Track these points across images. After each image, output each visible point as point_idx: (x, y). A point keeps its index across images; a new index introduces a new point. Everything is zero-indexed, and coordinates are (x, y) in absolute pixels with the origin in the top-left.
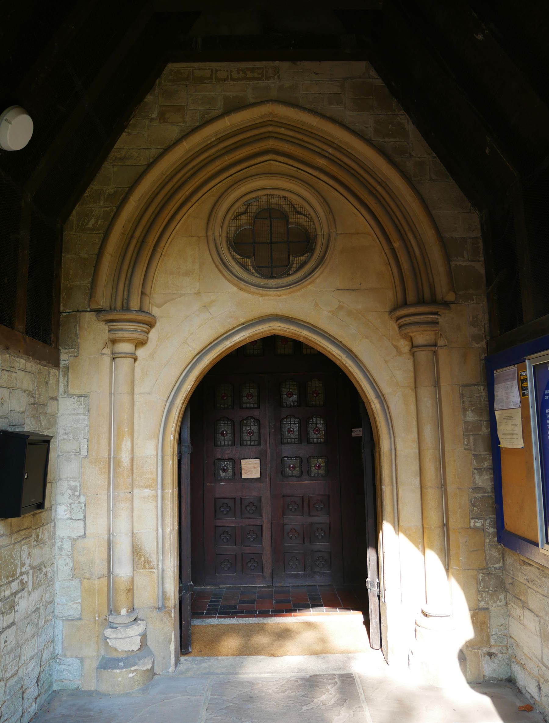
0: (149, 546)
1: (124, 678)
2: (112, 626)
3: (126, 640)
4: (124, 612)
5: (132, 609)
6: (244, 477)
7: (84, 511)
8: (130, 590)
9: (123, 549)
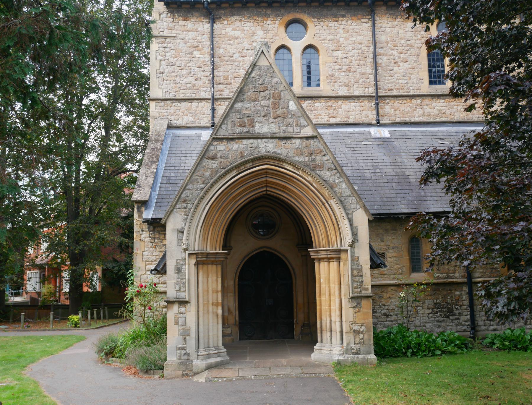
8: (228, 319)
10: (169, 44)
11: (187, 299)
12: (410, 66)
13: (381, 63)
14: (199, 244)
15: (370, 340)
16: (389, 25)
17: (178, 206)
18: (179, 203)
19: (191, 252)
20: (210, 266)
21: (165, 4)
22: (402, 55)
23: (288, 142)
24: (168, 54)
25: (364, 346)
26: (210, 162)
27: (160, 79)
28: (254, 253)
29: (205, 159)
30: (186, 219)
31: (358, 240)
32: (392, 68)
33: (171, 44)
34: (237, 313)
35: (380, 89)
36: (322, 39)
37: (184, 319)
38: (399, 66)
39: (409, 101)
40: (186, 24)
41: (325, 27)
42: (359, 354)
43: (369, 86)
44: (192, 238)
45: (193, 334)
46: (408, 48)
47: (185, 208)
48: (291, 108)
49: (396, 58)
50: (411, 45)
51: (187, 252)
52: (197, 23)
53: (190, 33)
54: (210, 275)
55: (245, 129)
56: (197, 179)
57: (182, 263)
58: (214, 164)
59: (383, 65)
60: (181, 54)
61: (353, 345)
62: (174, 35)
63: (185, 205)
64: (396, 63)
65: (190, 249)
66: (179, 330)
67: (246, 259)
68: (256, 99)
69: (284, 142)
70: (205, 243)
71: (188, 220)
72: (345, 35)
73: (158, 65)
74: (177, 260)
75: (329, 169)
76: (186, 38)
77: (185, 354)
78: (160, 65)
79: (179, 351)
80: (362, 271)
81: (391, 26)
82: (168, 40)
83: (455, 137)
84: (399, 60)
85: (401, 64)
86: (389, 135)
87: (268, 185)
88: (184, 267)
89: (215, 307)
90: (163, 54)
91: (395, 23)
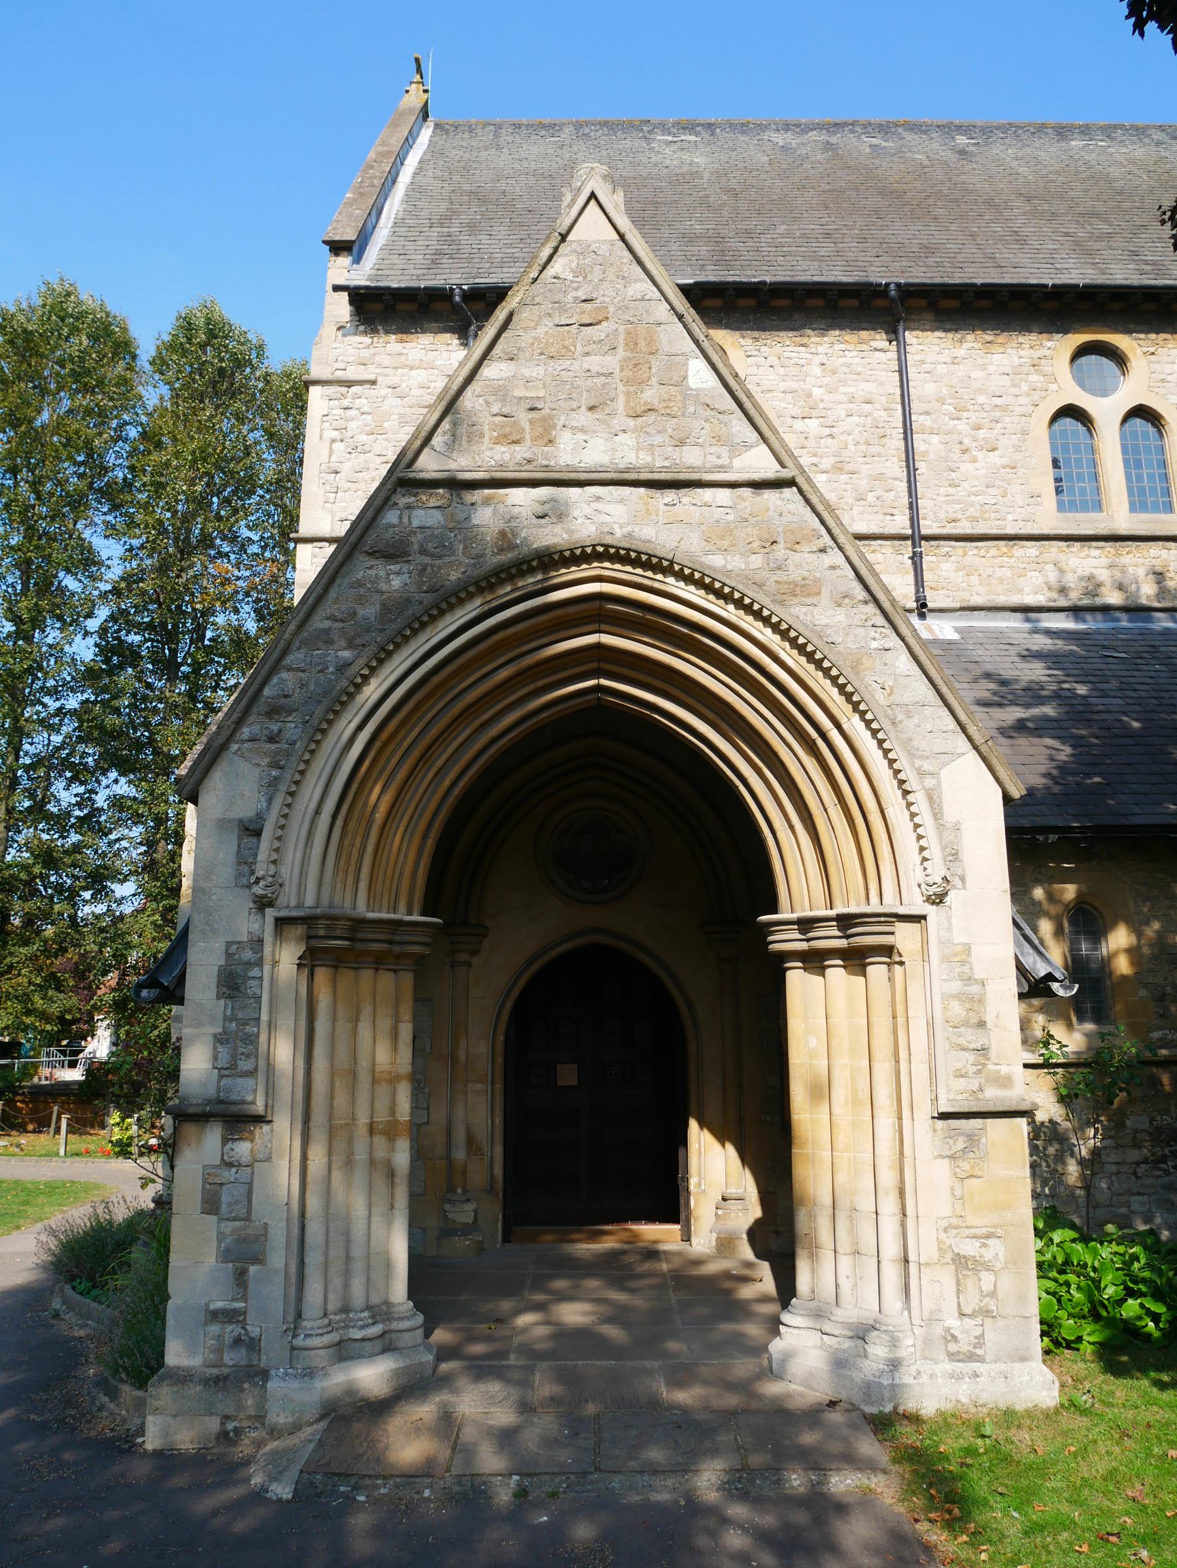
0: (482, 1134)
1: (462, 1244)
2: (449, 1201)
3: (463, 1214)
4: (459, 1191)
5: (465, 1190)
6: (559, 1084)
7: (428, 1101)
8: (464, 1173)
9: (460, 1134)
10: (358, 401)
11: (259, 1107)
12: (1004, 461)
13: (926, 452)
14: (320, 885)
15: (1022, 1298)
16: (946, 356)
17: (246, 732)
18: (251, 719)
19: (284, 913)
20: (367, 974)
21: (351, 302)
22: (982, 433)
23: (685, 500)
24: (352, 425)
25: (1001, 1323)
26: (380, 569)
27: (328, 487)
28: (562, 949)
29: (362, 557)
30: (274, 783)
31: (963, 879)
32: (957, 465)
33: (364, 401)
34: (499, 1150)
35: (925, 519)
36: (766, 388)
37: (243, 1189)
38: (974, 461)
39: (1005, 550)
40: (404, 351)
41: (773, 360)
42: (981, 1360)
43: (894, 511)
44: (292, 855)
45: (278, 1257)
46: (998, 414)
47: (271, 739)
48: (693, 382)
49: (966, 441)
50: (1005, 409)
51: (270, 913)
52: (434, 347)
53: (414, 373)
54: (367, 1010)
55: (521, 452)
56: (327, 631)
57: (248, 955)
58: (396, 580)
59: (932, 456)
60: (386, 424)
61: (953, 1322)
62: (372, 377)
63: (275, 727)
64: (965, 451)
65: (282, 900)
66: (221, 1237)
67: (534, 968)
68: (565, 353)
69: (667, 500)
70: (350, 880)
71: (283, 788)
72: (826, 380)
73: (326, 452)
74: (229, 944)
75: (841, 600)
76: (404, 385)
77: (238, 1341)
78: (331, 452)
79: (214, 1329)
80: (981, 1000)
81: (949, 360)
82: (354, 389)
83: (1142, 643)
84: (974, 444)
85: (980, 455)
86: (956, 636)
87: (604, 666)
88: (255, 972)
89: (380, 1142)
90: (341, 424)
91: (961, 352)
